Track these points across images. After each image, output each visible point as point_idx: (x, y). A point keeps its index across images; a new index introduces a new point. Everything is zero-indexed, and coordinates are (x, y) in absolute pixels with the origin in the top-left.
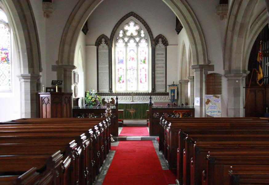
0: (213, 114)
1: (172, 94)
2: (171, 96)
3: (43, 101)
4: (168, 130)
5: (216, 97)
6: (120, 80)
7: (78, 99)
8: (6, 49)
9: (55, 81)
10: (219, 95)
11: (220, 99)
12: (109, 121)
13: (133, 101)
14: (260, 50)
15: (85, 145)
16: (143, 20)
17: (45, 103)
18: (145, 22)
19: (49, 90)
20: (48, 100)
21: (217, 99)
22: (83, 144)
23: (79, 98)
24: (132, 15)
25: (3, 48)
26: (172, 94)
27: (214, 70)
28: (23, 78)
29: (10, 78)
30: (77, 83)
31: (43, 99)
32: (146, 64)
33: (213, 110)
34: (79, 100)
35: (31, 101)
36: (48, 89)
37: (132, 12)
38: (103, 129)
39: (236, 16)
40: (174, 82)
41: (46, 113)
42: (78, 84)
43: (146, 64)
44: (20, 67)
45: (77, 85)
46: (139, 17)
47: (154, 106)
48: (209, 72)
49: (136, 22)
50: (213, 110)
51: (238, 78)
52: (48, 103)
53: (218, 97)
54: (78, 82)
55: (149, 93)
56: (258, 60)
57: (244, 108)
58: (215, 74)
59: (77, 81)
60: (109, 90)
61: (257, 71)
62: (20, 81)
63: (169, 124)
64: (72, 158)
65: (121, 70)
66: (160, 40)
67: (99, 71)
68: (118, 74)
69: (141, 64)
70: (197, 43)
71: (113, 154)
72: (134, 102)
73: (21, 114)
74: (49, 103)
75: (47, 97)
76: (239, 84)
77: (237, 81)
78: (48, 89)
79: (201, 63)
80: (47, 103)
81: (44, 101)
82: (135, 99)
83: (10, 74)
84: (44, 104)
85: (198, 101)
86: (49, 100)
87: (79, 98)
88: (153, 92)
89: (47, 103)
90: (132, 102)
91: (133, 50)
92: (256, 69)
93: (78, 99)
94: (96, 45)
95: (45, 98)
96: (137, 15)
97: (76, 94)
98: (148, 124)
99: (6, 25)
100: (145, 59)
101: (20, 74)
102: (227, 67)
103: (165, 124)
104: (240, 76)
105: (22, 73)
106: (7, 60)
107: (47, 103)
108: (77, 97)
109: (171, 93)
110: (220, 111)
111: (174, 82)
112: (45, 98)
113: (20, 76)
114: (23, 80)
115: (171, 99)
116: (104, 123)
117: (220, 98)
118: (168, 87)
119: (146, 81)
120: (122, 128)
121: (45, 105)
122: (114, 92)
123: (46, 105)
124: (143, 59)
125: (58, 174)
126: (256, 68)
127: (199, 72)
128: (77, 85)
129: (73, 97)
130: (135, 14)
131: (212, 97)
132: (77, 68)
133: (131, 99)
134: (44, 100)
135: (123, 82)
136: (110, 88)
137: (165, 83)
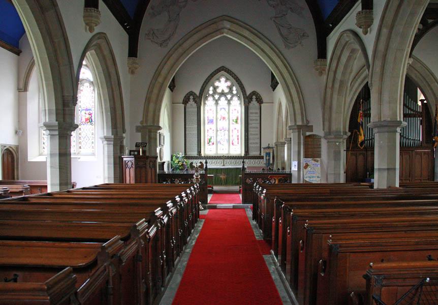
0: (311, 179)
1: (268, 158)
2: (266, 160)
4: (262, 197)
5: (315, 161)
6: (210, 141)
7: (164, 162)
8: (90, 110)
10: (318, 159)
11: (319, 163)
15: (172, 213)
21: (316, 163)
26: (268, 158)
33: (312, 175)
39: (335, 72)
44: (104, 129)
48: (308, 134)
50: (312, 175)
51: (339, 140)
53: (318, 162)
55: (241, 156)
56: (359, 121)
57: (345, 173)
58: (314, 135)
59: (162, 144)
61: (358, 133)
62: (103, 143)
64: (158, 227)
67: (187, 126)
68: (208, 135)
76: (339, 147)
77: (337, 144)
85: (295, 165)
86: (132, 164)
93: (164, 162)
94: (183, 103)
98: (240, 190)
104: (341, 138)
105: (105, 135)
108: (163, 161)
110: (320, 176)
117: (319, 161)
119: (238, 143)
122: (203, 155)
129: (159, 160)
131: (310, 161)
135: (213, 144)
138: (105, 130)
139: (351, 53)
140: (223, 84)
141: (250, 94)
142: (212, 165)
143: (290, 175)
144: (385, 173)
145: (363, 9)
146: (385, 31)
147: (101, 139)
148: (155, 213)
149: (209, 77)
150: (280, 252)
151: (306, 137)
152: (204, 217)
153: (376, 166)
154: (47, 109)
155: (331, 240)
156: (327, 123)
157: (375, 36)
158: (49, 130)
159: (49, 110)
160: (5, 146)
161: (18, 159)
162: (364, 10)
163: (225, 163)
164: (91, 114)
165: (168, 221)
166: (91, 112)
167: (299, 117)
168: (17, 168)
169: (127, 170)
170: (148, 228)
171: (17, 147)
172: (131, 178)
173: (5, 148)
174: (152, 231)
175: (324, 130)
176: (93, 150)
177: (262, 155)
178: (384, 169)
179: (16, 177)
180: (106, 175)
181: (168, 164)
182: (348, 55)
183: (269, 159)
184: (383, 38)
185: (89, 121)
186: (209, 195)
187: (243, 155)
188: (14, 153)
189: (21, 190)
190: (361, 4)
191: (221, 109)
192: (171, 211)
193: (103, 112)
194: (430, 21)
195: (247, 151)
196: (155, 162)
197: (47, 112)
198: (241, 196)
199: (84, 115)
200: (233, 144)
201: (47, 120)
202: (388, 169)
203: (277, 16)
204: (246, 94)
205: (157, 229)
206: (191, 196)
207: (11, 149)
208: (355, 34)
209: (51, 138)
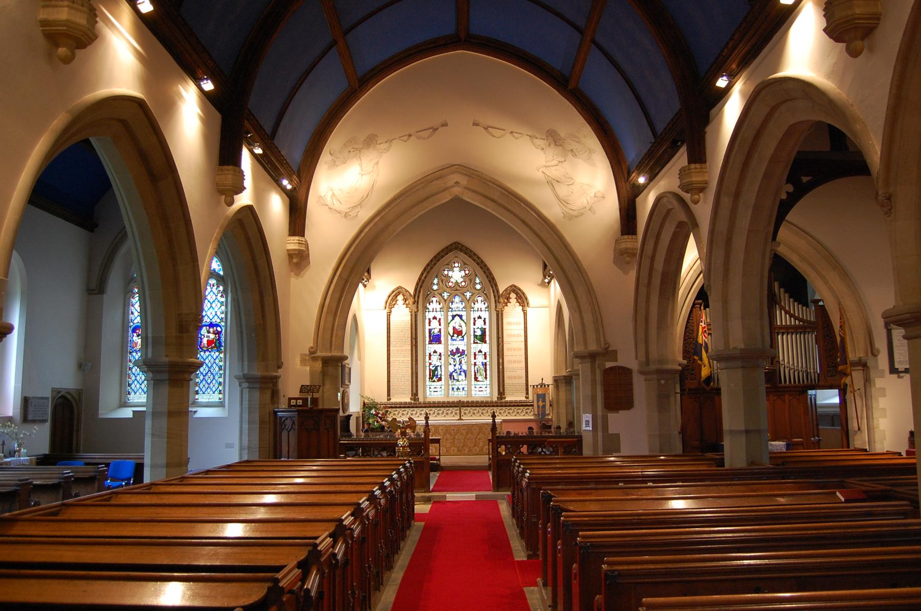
1: (541, 404)
2: (538, 406)
3: (283, 425)
4: (524, 483)
6: (434, 375)
7: (350, 416)
8: (217, 325)
9: (308, 386)
12: (411, 465)
13: (460, 419)
14: (702, 322)
15: (368, 519)
16: (479, 258)
17: (287, 429)
18: (482, 262)
19: (295, 401)
20: (291, 424)
22: (363, 516)
23: (351, 415)
24: (456, 248)
25: (211, 323)
26: (541, 404)
27: (617, 361)
28: (246, 382)
29: (221, 380)
30: (348, 385)
31: (282, 421)
32: (485, 342)
34: (351, 418)
35: (260, 424)
36: (292, 401)
37: (456, 242)
38: (399, 483)
39: (652, 259)
40: (542, 379)
41: (287, 448)
42: (350, 386)
43: (485, 342)
44: (243, 361)
45: (347, 390)
46: (471, 251)
47: (502, 431)
48: (609, 365)
49: (464, 261)
52: (292, 430)
54: (350, 382)
55: (492, 402)
56: (700, 342)
57: (680, 433)
58: (620, 368)
59: (347, 382)
60: (412, 395)
61: (699, 362)
62: (240, 385)
63: (527, 472)
64: (347, 544)
65: (435, 358)
66: (513, 296)
68: (430, 364)
69: (477, 343)
70: (582, 309)
71: (137, 306)
72: (462, 420)
73: (241, 449)
74: (294, 429)
75: (290, 417)
78: (292, 401)
79: (593, 347)
80: (291, 429)
81: (285, 425)
82: (465, 413)
83: (222, 372)
84: (285, 430)
85: (588, 421)
86: (293, 423)
87: (351, 415)
88: (501, 398)
89: (291, 429)
90: (458, 420)
91: (459, 315)
92: (696, 357)
93: (350, 416)
95: (286, 419)
96: (467, 248)
97: (346, 407)
98: (490, 465)
99: (219, 280)
100: (484, 331)
101: (241, 374)
102: (642, 352)
103: (519, 473)
105: (246, 372)
106: (218, 345)
107: (290, 428)
108: (347, 414)
109: (538, 401)
111: (542, 379)
112: (286, 419)
113: (242, 377)
114: (245, 385)
115: (539, 413)
116: (401, 470)
118: (530, 389)
119: (486, 378)
120: (437, 474)
121: (286, 432)
122: (421, 400)
123: (289, 432)
124: (479, 333)
125: (327, 571)
126: (697, 356)
127: (590, 364)
128: (347, 390)
129: (341, 413)
130: (462, 246)
132: (349, 357)
133: (456, 414)
134: (285, 423)
135: (440, 379)
136: (414, 391)
137: (524, 382)
138: (246, 363)
139: (677, 227)
140: (457, 275)
141: (506, 290)
142: (438, 419)
143: (579, 439)
144: (743, 439)
145: (690, 162)
146: (726, 202)
147: (237, 378)
148: (342, 521)
149: (431, 261)
150: (550, 581)
151: (607, 372)
152: (422, 517)
153: (726, 426)
154: (150, 335)
155: (606, 565)
156: (642, 346)
157: (632, 308)
158: (152, 372)
159: (153, 338)
160: (59, 392)
161: (79, 414)
162: (693, 166)
163: (462, 414)
164: (219, 333)
165: (362, 531)
166: (219, 329)
167: (591, 335)
168: (78, 431)
169: (284, 434)
170: (333, 546)
171: (80, 392)
172: (291, 449)
173: (60, 395)
174: (24, 432)
175: (636, 359)
176: (221, 396)
177: (531, 398)
178: (740, 432)
179: (74, 448)
180: (246, 442)
181: (357, 418)
182: (673, 230)
183: (544, 406)
184: (725, 212)
185: (214, 345)
186: (432, 474)
187: (495, 399)
188: (74, 404)
189: (92, 474)
190: (686, 153)
191: (454, 317)
192: (367, 514)
193: (242, 332)
194: (805, 179)
195: (501, 393)
196: (335, 417)
197: (150, 341)
198: (490, 474)
199: (206, 334)
200: (476, 379)
201: (150, 355)
202: (747, 432)
203: (548, 164)
204: (498, 291)
205: (346, 548)
206: (399, 483)
207: (69, 397)
208: (681, 201)
209: (154, 385)
